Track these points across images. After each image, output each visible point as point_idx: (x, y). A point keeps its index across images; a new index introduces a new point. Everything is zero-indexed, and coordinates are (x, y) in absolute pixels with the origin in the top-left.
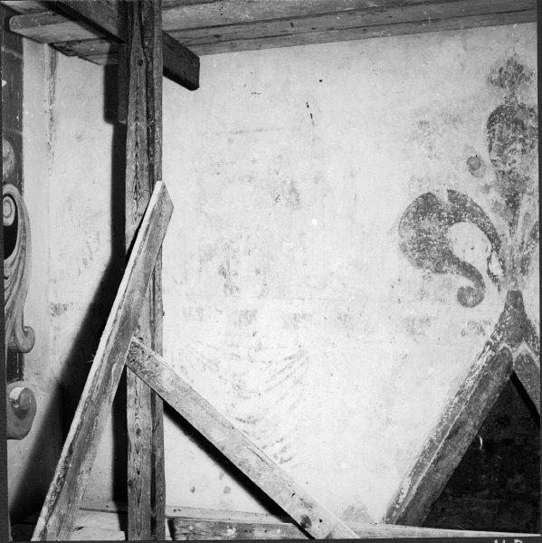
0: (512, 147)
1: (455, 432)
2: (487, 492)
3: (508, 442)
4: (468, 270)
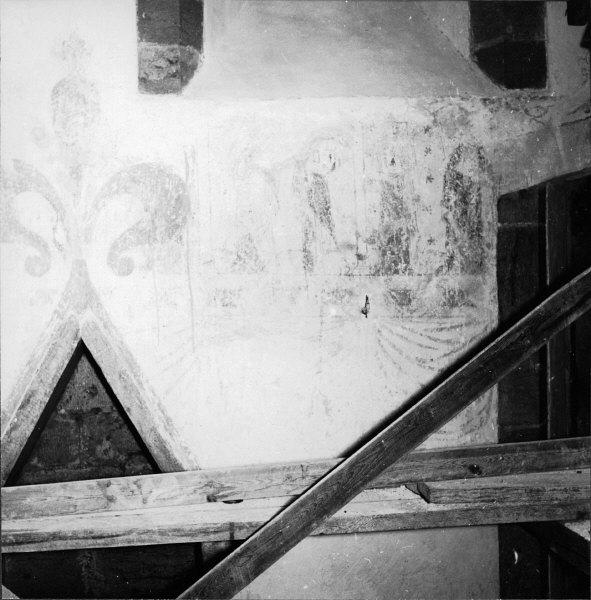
0: (75, 120)
1: (27, 401)
2: (77, 462)
3: (97, 410)
4: (35, 240)
